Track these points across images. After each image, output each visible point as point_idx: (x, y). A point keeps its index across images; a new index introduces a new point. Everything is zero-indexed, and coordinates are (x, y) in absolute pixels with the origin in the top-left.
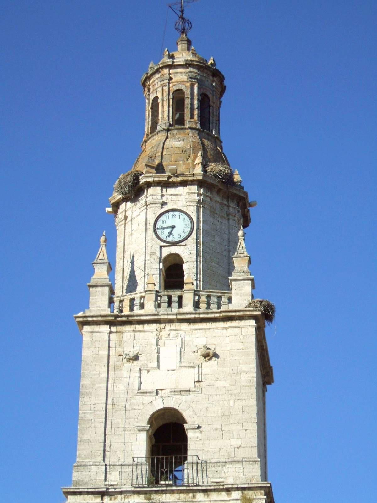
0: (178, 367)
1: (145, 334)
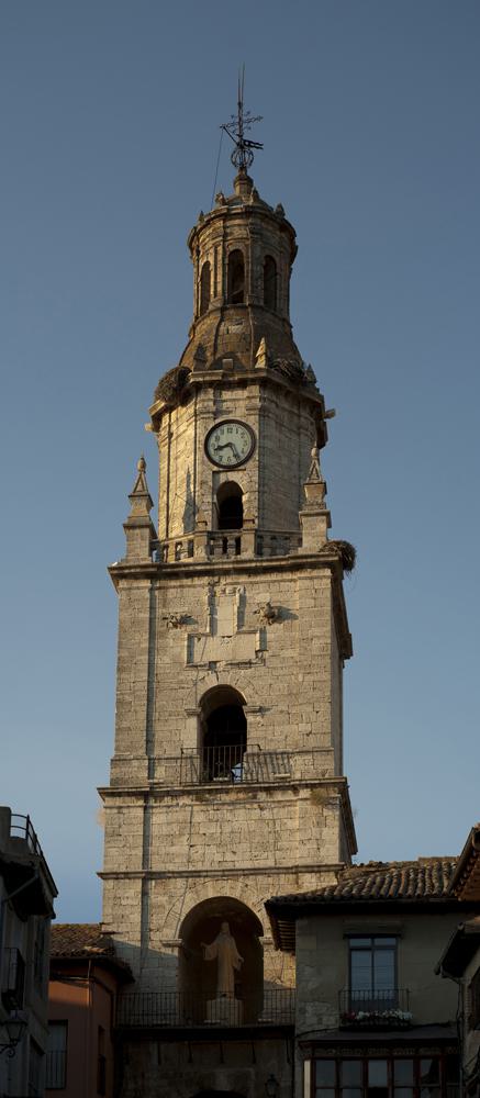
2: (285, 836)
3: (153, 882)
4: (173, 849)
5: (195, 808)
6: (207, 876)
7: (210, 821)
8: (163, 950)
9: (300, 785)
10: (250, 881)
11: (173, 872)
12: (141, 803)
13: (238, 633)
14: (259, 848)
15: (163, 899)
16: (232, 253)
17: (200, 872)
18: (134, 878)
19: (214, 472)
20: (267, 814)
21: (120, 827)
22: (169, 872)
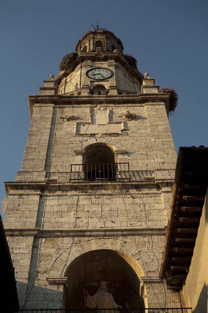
0: (107, 123)
1: (82, 109)
2: (154, 213)
3: (44, 240)
4: (62, 220)
5: (81, 197)
6: (90, 236)
7: (93, 204)
8: (49, 287)
9: (162, 183)
10: (129, 239)
11: (61, 232)
12: (39, 192)
13: (109, 123)
14: (133, 220)
15: (52, 251)
16: (97, 42)
17: (84, 231)
18: (28, 235)
19: (91, 81)
20: (137, 201)
21: (19, 205)
22: (58, 231)
